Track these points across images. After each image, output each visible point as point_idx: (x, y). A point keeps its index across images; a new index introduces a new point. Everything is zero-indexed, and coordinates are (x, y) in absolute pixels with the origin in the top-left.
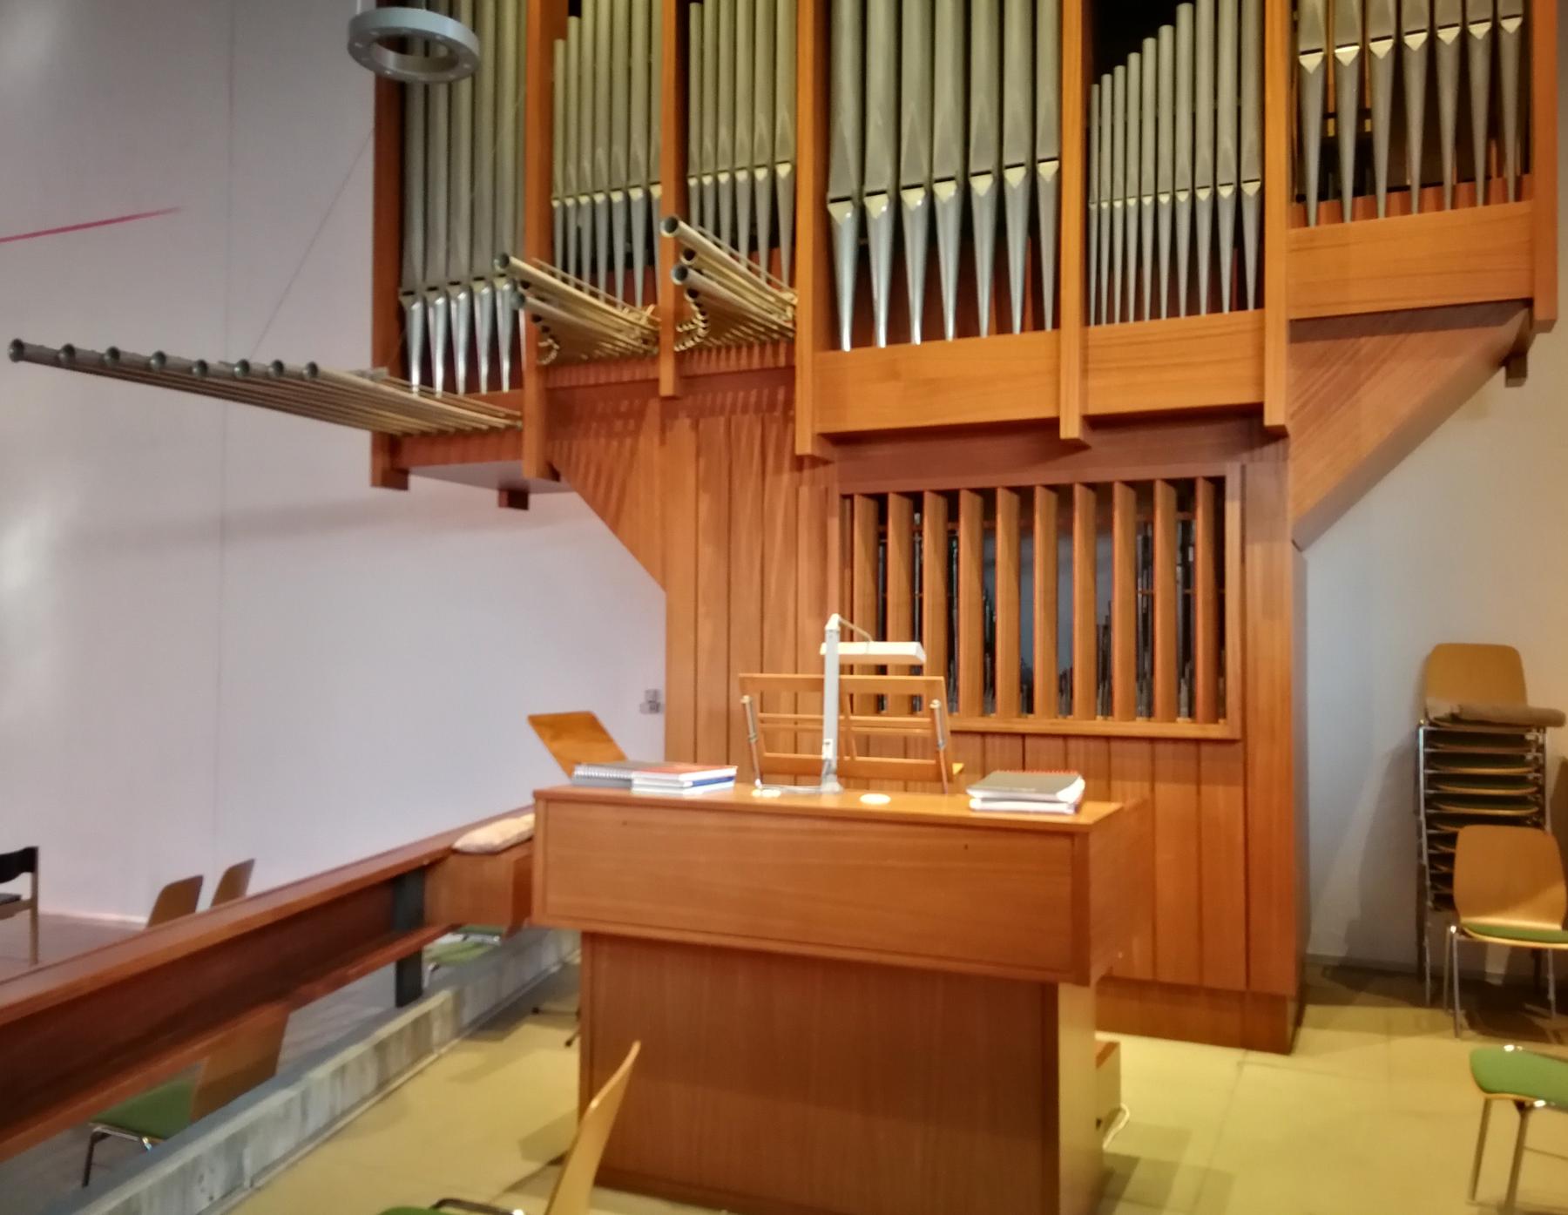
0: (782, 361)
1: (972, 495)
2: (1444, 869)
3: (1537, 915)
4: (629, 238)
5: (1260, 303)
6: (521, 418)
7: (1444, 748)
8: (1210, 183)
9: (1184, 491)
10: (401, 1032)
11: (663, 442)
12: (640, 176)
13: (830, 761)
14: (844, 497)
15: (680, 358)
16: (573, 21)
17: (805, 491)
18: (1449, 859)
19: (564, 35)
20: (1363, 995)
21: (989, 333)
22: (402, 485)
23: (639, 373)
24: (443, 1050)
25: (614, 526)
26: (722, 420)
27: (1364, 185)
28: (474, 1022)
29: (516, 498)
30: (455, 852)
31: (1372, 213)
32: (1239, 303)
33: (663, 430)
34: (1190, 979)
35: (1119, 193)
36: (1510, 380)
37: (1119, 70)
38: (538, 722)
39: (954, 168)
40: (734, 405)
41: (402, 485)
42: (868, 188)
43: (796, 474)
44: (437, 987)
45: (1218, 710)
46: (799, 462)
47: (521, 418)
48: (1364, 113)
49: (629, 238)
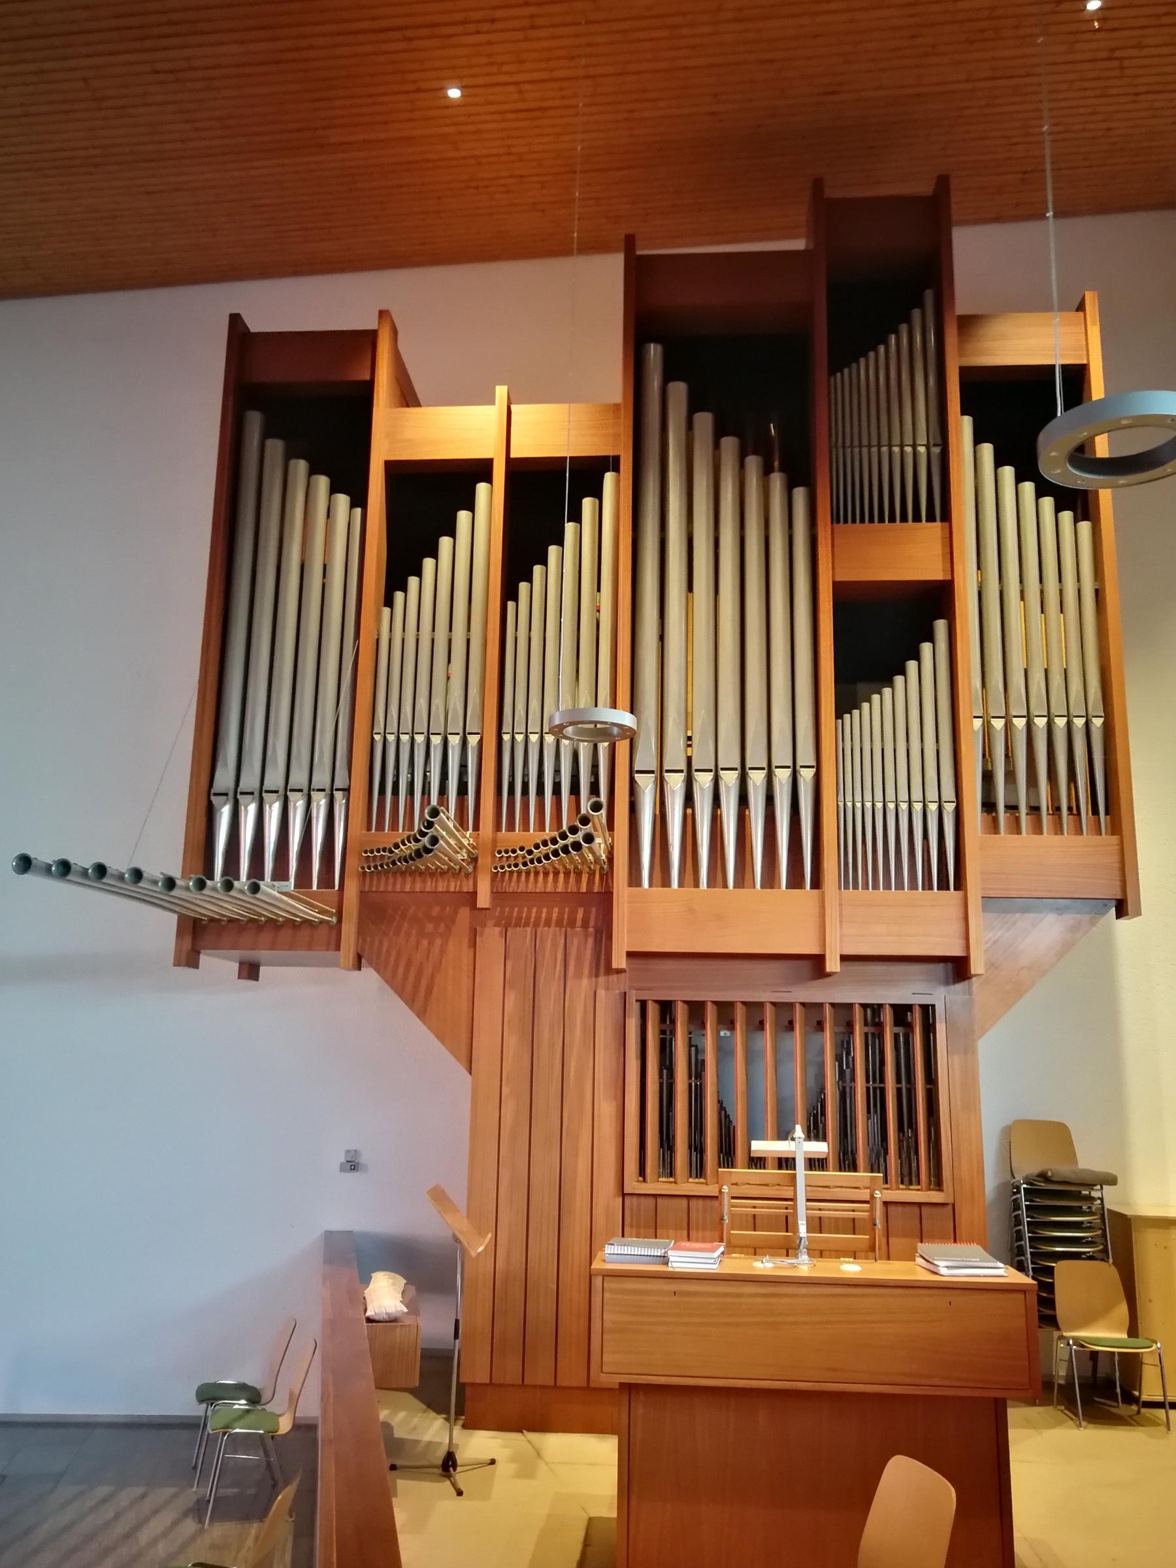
1: (654, 1004)
3: (1111, 1328)
7: (1040, 1202)
18: (1050, 1288)
25: (422, 1014)
26: (529, 929)
40: (538, 918)
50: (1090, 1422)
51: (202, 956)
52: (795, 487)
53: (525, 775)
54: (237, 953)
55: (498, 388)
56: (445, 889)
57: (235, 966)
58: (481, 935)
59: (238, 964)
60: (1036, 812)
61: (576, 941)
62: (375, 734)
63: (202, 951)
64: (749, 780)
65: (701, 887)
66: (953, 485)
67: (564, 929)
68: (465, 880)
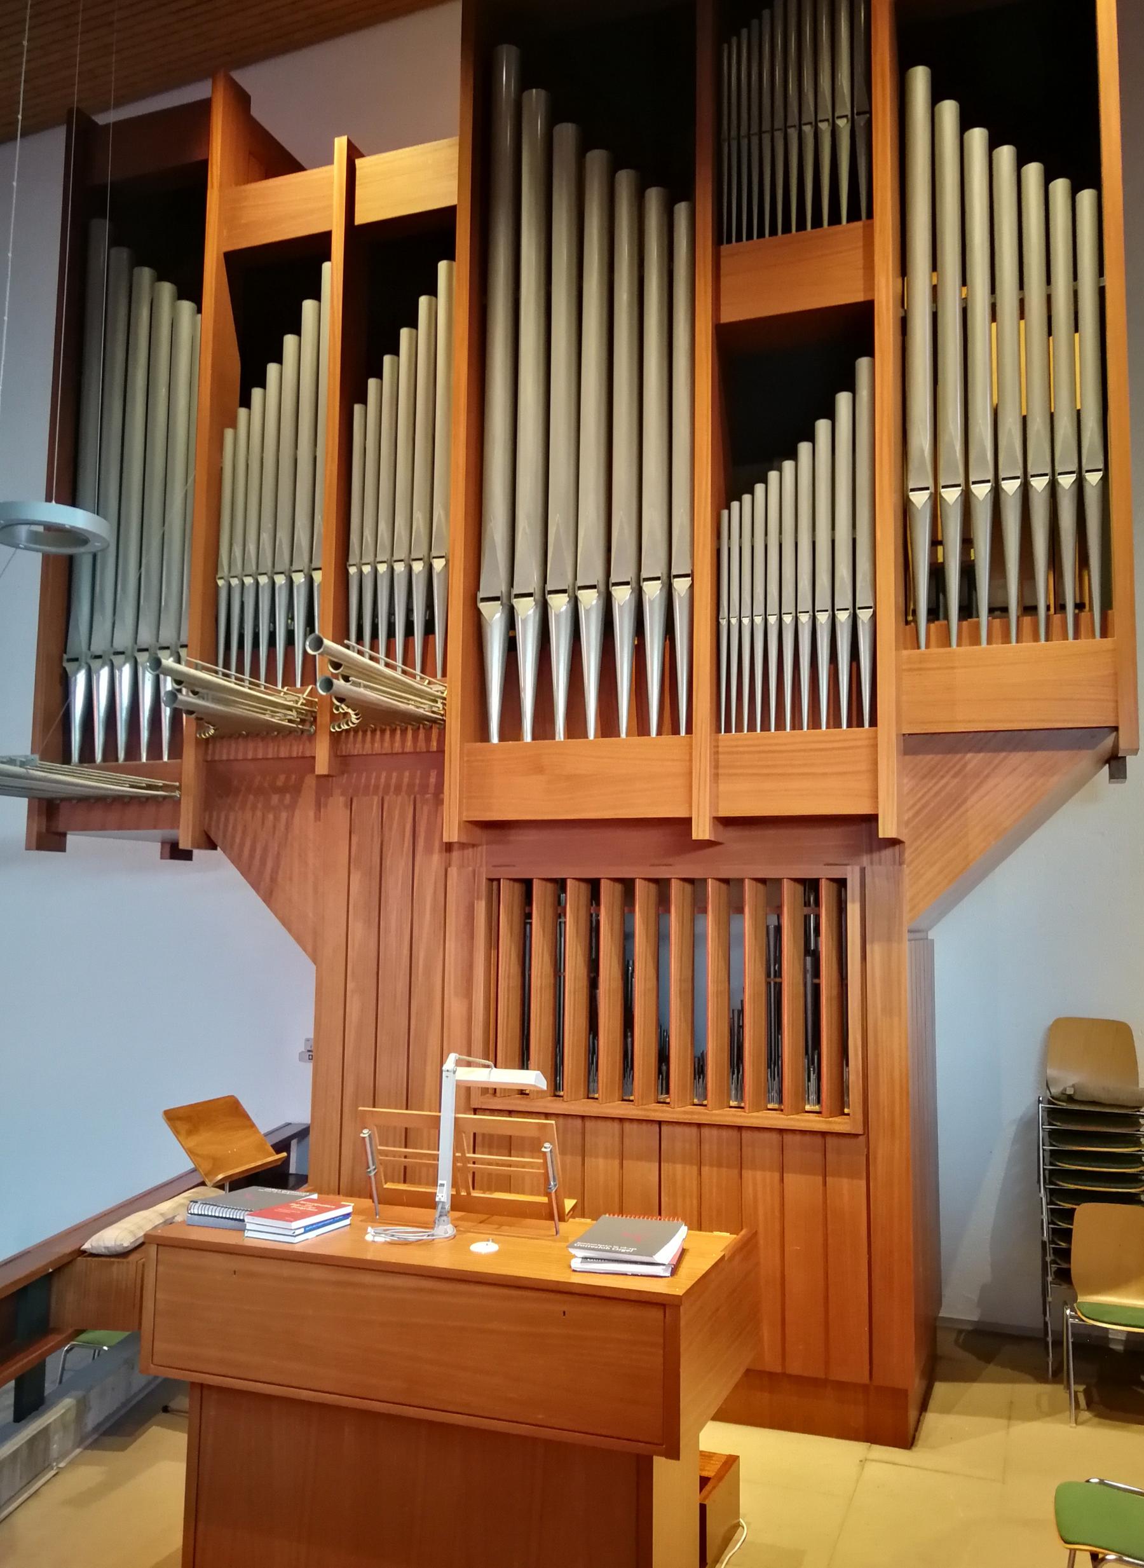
0: (434, 746)
2: (1063, 1245)
4: (290, 616)
5: (873, 722)
6: (179, 788)
8: (829, 607)
9: (811, 886)
10: (15, 1455)
11: (317, 818)
12: (301, 561)
13: (443, 1202)
14: (491, 880)
15: (336, 738)
16: (242, 412)
17: (453, 871)
18: (1067, 1235)
19: (234, 424)
20: (992, 1368)
21: (628, 735)
22: (61, 847)
23: (296, 750)
24: (62, 1465)
25: (268, 898)
26: (376, 800)
27: (968, 610)
28: (96, 1429)
29: (176, 852)
30: (83, 1253)
31: (975, 640)
32: (856, 719)
33: (318, 806)
34: (815, 1371)
35: (746, 611)
36: (1112, 780)
37: (747, 498)
38: (173, 1117)
39: (597, 577)
40: (387, 785)
41: (61, 847)
42: (516, 590)
43: (448, 854)
44: (60, 1395)
45: (840, 1106)
46: (449, 847)
47: (179, 788)
48: (967, 542)
49: (290, 616)
50: (1099, 1415)
51: (69, 837)
52: (676, 203)
53: (391, 613)
54: (158, 833)
55: (337, 140)
56: (287, 755)
57: (158, 846)
58: (326, 805)
59: (160, 844)
60: (1004, 614)
61: (426, 809)
62: (484, 600)
63: (68, 832)
64: (858, 619)
65: (557, 739)
66: (877, 166)
67: (412, 797)
68: (307, 742)
